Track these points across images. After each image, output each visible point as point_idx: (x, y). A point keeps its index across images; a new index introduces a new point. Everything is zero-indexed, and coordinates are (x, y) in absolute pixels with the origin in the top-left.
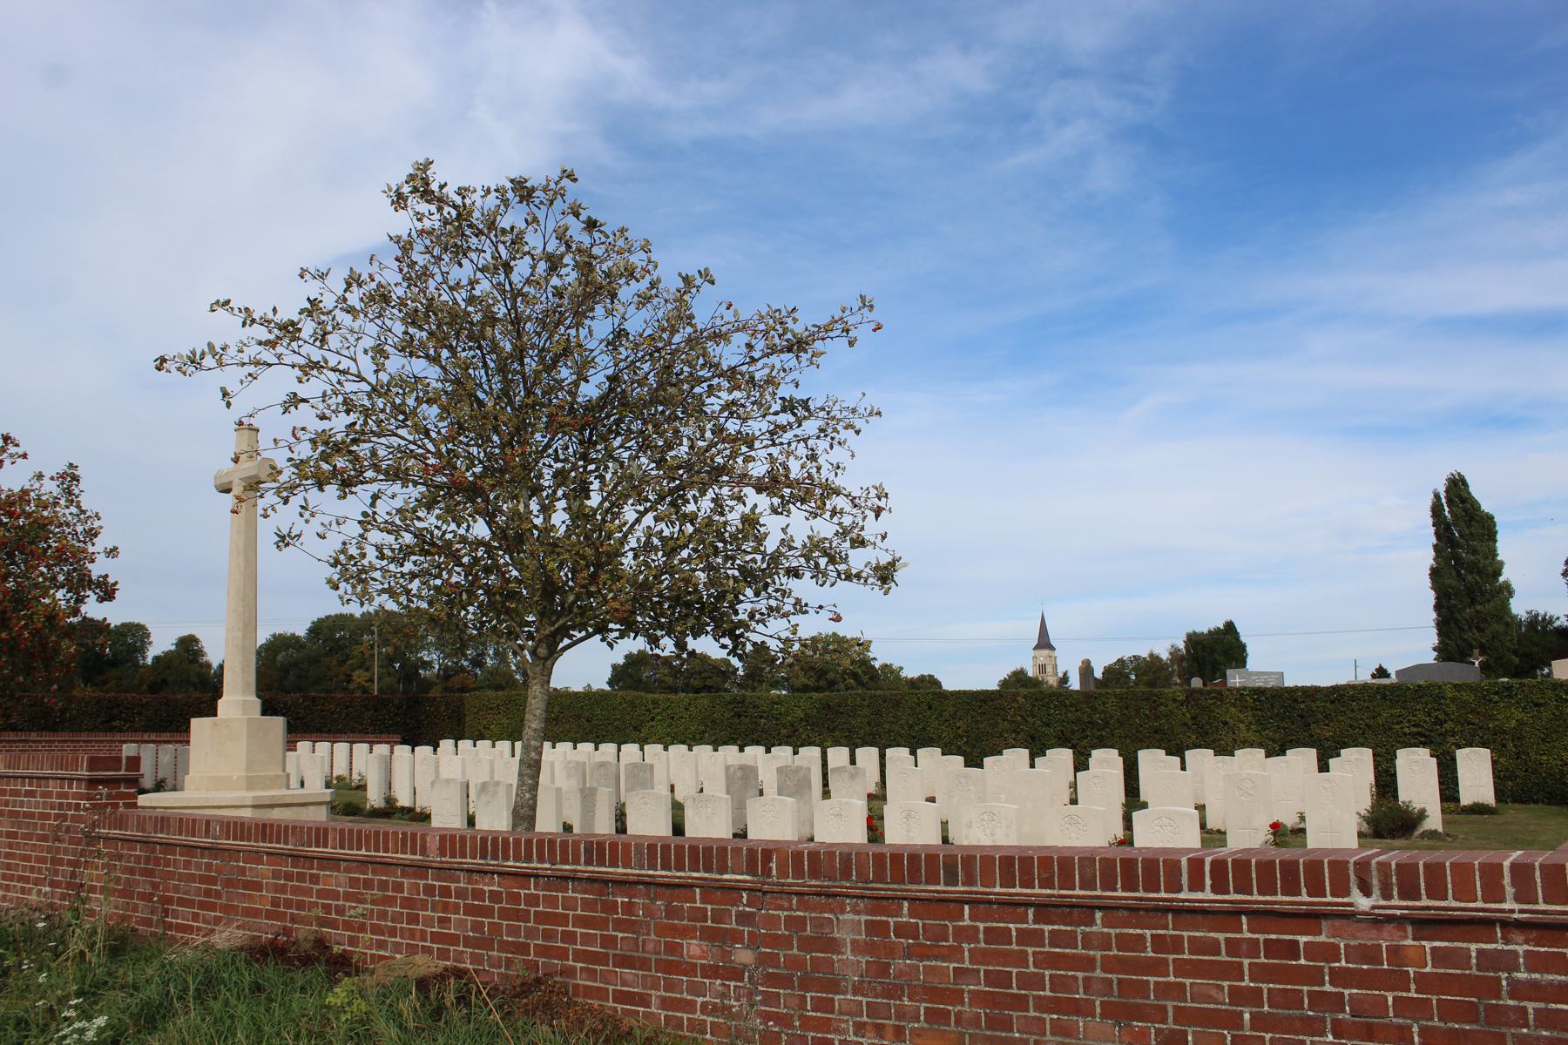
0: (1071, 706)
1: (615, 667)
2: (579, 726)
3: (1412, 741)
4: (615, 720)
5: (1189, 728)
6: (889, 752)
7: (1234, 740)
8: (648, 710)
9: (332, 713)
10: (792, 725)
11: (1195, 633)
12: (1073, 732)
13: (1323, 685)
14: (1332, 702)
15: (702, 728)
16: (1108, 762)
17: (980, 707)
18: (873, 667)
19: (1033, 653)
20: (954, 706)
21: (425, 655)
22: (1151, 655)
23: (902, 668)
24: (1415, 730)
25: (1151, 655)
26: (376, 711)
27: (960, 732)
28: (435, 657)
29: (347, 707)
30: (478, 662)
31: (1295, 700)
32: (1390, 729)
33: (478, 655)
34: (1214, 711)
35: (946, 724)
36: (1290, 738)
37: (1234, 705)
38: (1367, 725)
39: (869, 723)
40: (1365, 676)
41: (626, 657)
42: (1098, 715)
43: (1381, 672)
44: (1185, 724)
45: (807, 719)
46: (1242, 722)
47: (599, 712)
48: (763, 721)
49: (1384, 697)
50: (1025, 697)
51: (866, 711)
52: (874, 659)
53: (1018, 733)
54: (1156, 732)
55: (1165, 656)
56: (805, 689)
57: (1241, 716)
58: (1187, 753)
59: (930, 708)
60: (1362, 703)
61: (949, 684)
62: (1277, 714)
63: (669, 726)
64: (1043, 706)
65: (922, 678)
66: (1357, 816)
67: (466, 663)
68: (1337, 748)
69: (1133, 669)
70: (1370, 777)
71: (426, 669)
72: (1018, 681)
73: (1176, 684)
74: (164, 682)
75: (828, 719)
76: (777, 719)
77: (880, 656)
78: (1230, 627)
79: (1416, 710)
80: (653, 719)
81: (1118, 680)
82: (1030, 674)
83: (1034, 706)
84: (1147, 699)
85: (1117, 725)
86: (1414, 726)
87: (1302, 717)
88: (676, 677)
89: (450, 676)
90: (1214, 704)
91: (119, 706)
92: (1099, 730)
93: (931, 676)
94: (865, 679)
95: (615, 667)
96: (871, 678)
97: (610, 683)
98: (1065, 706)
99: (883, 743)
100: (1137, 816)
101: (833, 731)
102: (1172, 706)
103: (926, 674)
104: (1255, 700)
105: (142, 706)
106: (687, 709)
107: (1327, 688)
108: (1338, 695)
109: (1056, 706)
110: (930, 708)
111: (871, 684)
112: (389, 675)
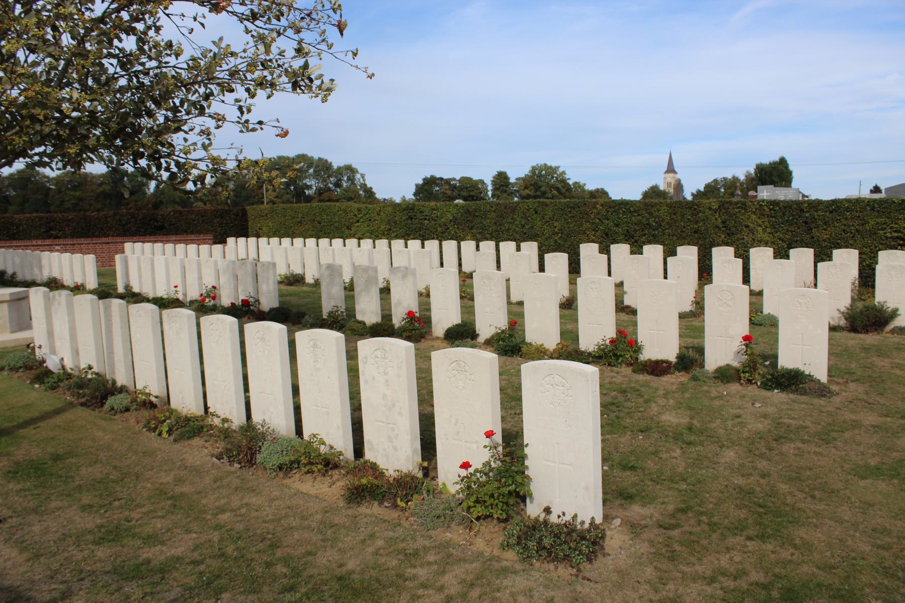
0: (635, 211)
1: (417, 186)
2: (314, 227)
3: (893, 243)
4: (336, 222)
5: (720, 229)
6: (502, 244)
7: (753, 239)
8: (355, 215)
9: (194, 220)
10: (445, 225)
11: (761, 164)
12: (635, 231)
13: (824, 199)
14: (831, 212)
15: (388, 227)
16: (688, 254)
17: (570, 212)
18: (568, 184)
19: (664, 176)
20: (552, 211)
21: (308, 182)
22: (734, 177)
23: (585, 184)
24: (895, 235)
25: (734, 177)
26: (222, 218)
27: (556, 230)
28: (313, 183)
29: (203, 216)
30: (338, 185)
31: (802, 210)
32: (876, 233)
33: (338, 180)
34: (739, 218)
35: (547, 224)
36: (796, 239)
37: (755, 213)
38: (857, 230)
39: (495, 223)
40: (865, 193)
41: (424, 179)
42: (653, 219)
43: (876, 190)
44: (717, 227)
45: (455, 220)
46: (760, 226)
47: (325, 217)
48: (426, 222)
49: (873, 209)
50: (602, 205)
51: (494, 215)
52: (569, 179)
53: (597, 231)
54: (695, 232)
55: (742, 178)
56: (528, 197)
57: (760, 222)
58: (753, 251)
59: (536, 213)
60: (855, 213)
61: (616, 195)
62: (787, 220)
63: (368, 226)
64: (615, 211)
65: (597, 191)
66: (837, 312)
67: (331, 186)
68: (831, 247)
69: (723, 185)
70: (855, 272)
71: (308, 190)
72: (654, 192)
73: (738, 195)
74: (161, 202)
75: (468, 221)
76: (436, 221)
77: (572, 178)
78: (783, 161)
79: (898, 219)
80: (358, 221)
81: (713, 192)
82: (662, 188)
83: (608, 212)
84: (690, 208)
85: (667, 227)
86: (895, 231)
87: (806, 223)
88: (453, 191)
89: (322, 194)
90: (740, 212)
91: (53, 221)
92: (654, 230)
93: (602, 189)
94: (563, 191)
95: (417, 186)
96: (567, 190)
97: (415, 195)
98: (630, 212)
99: (498, 238)
100: (20, 277)
101: (471, 228)
102: (708, 213)
103: (599, 187)
104: (771, 210)
105: (69, 220)
106: (378, 214)
107: (828, 201)
108: (835, 206)
109: (624, 212)
110: (536, 213)
111: (567, 194)
112: (287, 193)
